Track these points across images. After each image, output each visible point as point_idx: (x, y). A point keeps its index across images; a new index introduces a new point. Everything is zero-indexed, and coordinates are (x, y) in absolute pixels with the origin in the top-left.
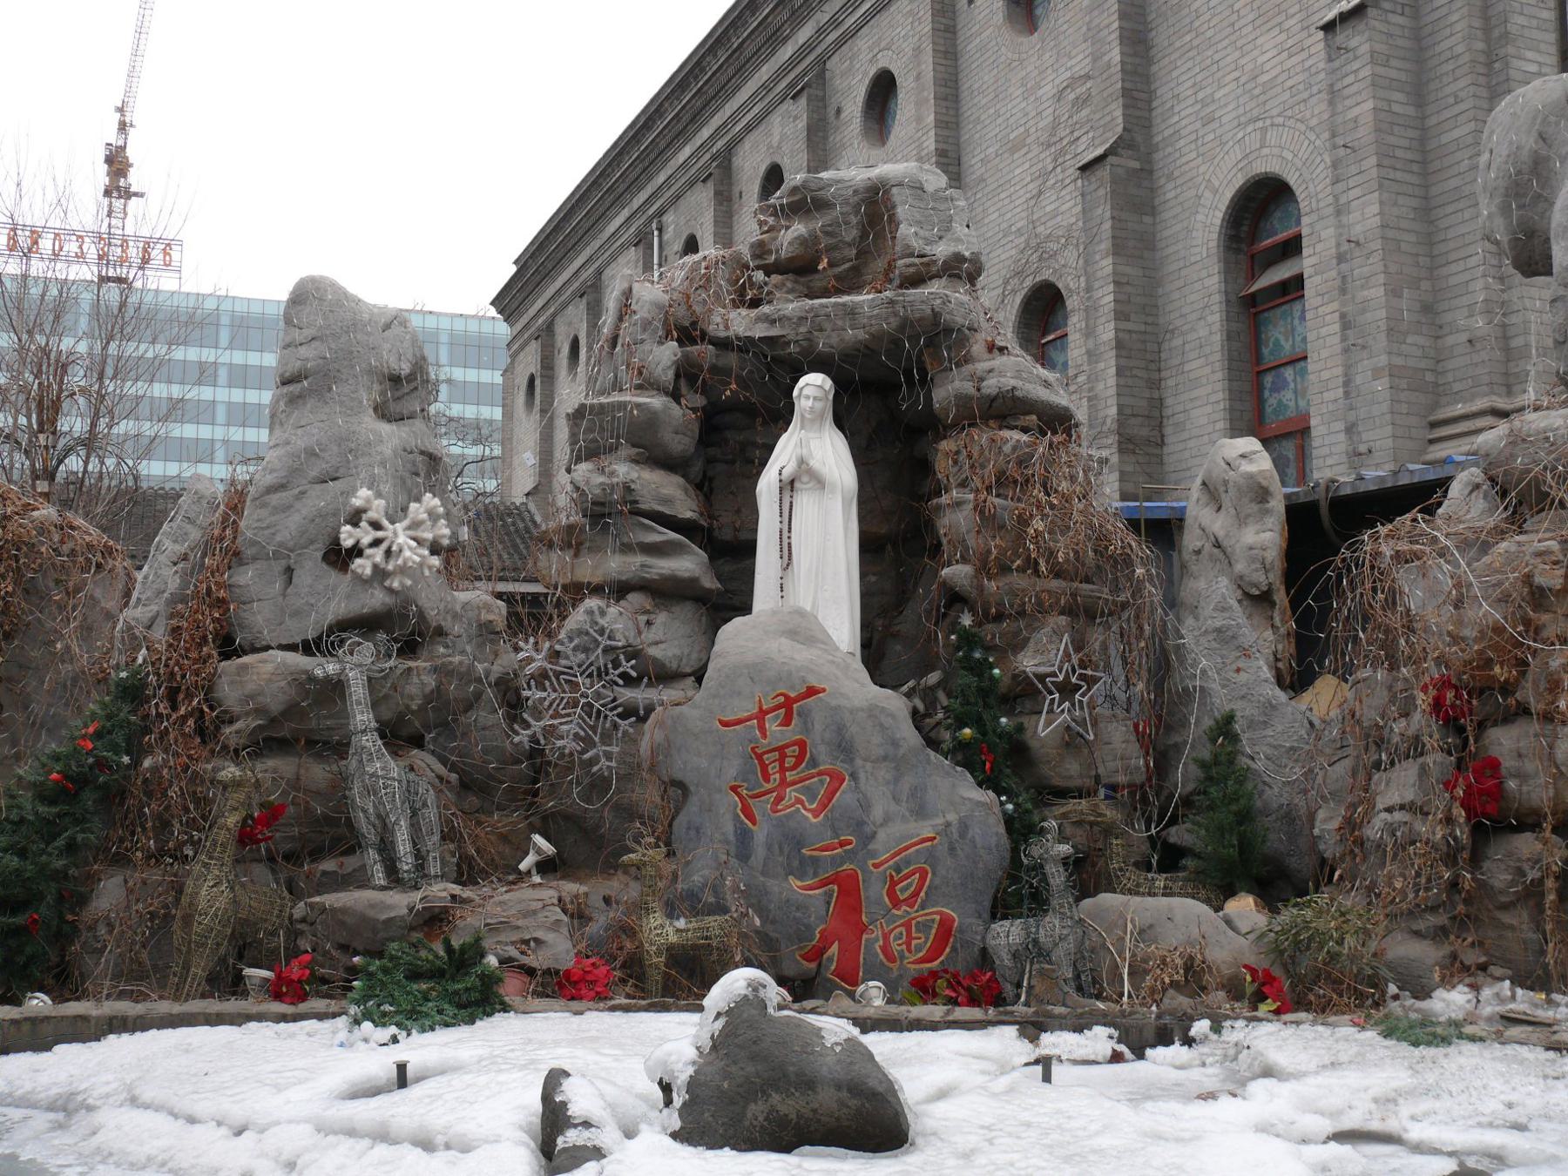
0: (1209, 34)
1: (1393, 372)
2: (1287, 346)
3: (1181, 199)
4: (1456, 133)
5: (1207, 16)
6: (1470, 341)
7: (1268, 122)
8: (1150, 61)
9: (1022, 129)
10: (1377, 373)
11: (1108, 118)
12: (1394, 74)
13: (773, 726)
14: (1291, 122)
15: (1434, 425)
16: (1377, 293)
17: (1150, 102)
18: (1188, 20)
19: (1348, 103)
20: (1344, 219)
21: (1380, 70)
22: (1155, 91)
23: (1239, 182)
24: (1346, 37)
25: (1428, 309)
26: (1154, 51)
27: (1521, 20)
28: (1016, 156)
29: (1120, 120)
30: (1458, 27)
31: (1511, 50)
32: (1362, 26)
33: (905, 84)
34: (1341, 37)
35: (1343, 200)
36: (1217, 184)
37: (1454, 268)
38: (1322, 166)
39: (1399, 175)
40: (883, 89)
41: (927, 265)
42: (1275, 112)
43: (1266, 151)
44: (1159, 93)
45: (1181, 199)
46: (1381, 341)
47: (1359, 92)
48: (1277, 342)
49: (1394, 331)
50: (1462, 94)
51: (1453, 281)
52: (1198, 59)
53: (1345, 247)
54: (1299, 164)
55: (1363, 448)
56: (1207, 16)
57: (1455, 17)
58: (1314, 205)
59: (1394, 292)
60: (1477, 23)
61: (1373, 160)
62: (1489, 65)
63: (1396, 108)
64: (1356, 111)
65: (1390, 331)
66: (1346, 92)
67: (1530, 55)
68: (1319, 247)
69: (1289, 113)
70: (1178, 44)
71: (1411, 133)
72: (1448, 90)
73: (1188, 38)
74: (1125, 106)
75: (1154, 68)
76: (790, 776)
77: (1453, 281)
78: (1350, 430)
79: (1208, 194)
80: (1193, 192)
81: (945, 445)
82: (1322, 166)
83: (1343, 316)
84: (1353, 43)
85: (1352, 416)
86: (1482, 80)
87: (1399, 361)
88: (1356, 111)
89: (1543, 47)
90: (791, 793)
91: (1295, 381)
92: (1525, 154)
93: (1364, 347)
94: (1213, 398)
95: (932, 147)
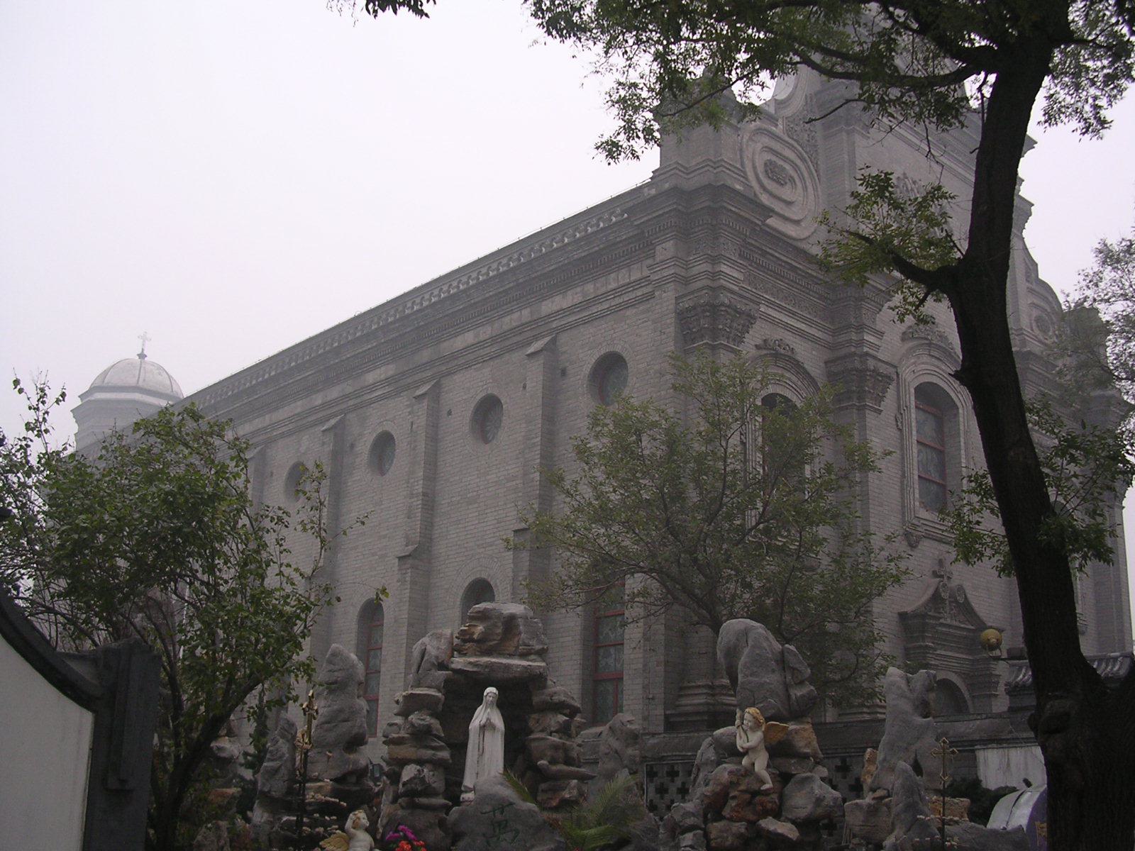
2: (612, 636)
9: (475, 493)
13: (498, 814)
28: (470, 507)
33: (401, 446)
40: (384, 444)
41: (530, 650)
48: (607, 634)
74: (540, 504)
81: (533, 716)
92: (732, 643)
94: (574, 658)
95: (421, 490)
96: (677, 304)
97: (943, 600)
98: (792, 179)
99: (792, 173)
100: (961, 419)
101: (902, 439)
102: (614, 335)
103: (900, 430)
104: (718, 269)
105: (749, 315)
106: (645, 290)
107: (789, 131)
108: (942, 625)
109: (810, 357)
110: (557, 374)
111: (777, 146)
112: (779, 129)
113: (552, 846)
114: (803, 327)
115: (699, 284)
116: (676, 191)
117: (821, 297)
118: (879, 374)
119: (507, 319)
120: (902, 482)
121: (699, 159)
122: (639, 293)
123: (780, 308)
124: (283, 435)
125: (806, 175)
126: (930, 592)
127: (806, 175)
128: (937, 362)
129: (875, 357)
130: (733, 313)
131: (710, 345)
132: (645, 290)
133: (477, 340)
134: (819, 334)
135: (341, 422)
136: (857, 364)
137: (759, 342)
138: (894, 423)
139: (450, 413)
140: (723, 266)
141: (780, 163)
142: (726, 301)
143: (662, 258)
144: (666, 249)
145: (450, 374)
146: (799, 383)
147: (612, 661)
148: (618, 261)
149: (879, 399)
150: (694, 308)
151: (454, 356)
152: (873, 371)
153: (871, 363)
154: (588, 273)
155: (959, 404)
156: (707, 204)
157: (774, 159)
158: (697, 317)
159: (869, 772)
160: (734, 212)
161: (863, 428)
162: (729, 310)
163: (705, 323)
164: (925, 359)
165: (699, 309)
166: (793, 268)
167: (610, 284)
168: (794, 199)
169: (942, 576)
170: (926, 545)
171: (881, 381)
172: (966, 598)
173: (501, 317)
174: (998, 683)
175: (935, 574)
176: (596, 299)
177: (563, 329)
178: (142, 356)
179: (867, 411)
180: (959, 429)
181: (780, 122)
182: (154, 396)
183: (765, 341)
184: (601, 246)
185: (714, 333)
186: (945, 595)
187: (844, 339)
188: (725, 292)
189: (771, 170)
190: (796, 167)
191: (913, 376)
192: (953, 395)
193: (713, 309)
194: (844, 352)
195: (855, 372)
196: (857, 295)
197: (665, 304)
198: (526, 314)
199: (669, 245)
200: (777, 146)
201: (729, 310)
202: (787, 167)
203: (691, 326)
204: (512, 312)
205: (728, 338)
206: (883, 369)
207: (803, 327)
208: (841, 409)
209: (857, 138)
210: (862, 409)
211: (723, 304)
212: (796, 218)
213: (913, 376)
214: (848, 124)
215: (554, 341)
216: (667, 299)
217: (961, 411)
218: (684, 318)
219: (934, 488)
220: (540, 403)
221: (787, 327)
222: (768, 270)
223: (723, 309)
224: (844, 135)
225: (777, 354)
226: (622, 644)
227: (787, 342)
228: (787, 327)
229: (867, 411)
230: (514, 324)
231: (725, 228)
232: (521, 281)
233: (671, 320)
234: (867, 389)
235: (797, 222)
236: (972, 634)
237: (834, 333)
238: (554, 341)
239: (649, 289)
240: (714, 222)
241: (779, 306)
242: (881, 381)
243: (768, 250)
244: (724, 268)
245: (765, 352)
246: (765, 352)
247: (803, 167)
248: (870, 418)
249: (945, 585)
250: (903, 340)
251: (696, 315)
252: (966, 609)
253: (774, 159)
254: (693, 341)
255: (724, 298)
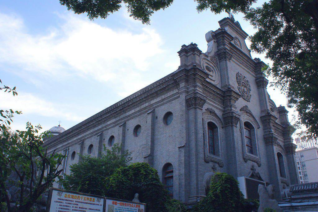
96: (186, 98)
98: (213, 71)
99: (212, 69)
105: (204, 100)
106: (177, 96)
109: (219, 113)
110: (154, 118)
111: (209, 63)
112: (209, 59)
118: (236, 117)
120: (242, 146)
122: (176, 96)
123: (211, 101)
124: (88, 138)
125: (215, 69)
126: (251, 174)
132: (177, 96)
135: (102, 134)
136: (231, 115)
137: (206, 109)
139: (128, 130)
141: (209, 66)
144: (182, 85)
145: (128, 120)
149: (236, 124)
150: (190, 98)
151: (129, 116)
152: (235, 117)
161: (233, 131)
163: (193, 102)
164: (246, 116)
169: (253, 170)
170: (249, 161)
172: (260, 176)
177: (156, 107)
178: (59, 126)
182: (105, 206)
183: (208, 108)
190: (213, 68)
193: (195, 98)
198: (147, 104)
199: (183, 83)
200: (209, 63)
204: (143, 104)
206: (237, 116)
209: (228, 62)
210: (232, 126)
212: (214, 80)
215: (154, 110)
216: (183, 97)
218: (187, 101)
219: (250, 148)
221: (213, 106)
225: (211, 112)
226: (173, 186)
228: (213, 106)
230: (144, 107)
233: (184, 102)
239: (178, 95)
247: (215, 68)
248: (234, 128)
249: (254, 172)
250: (240, 111)
253: (208, 65)
254: (190, 107)
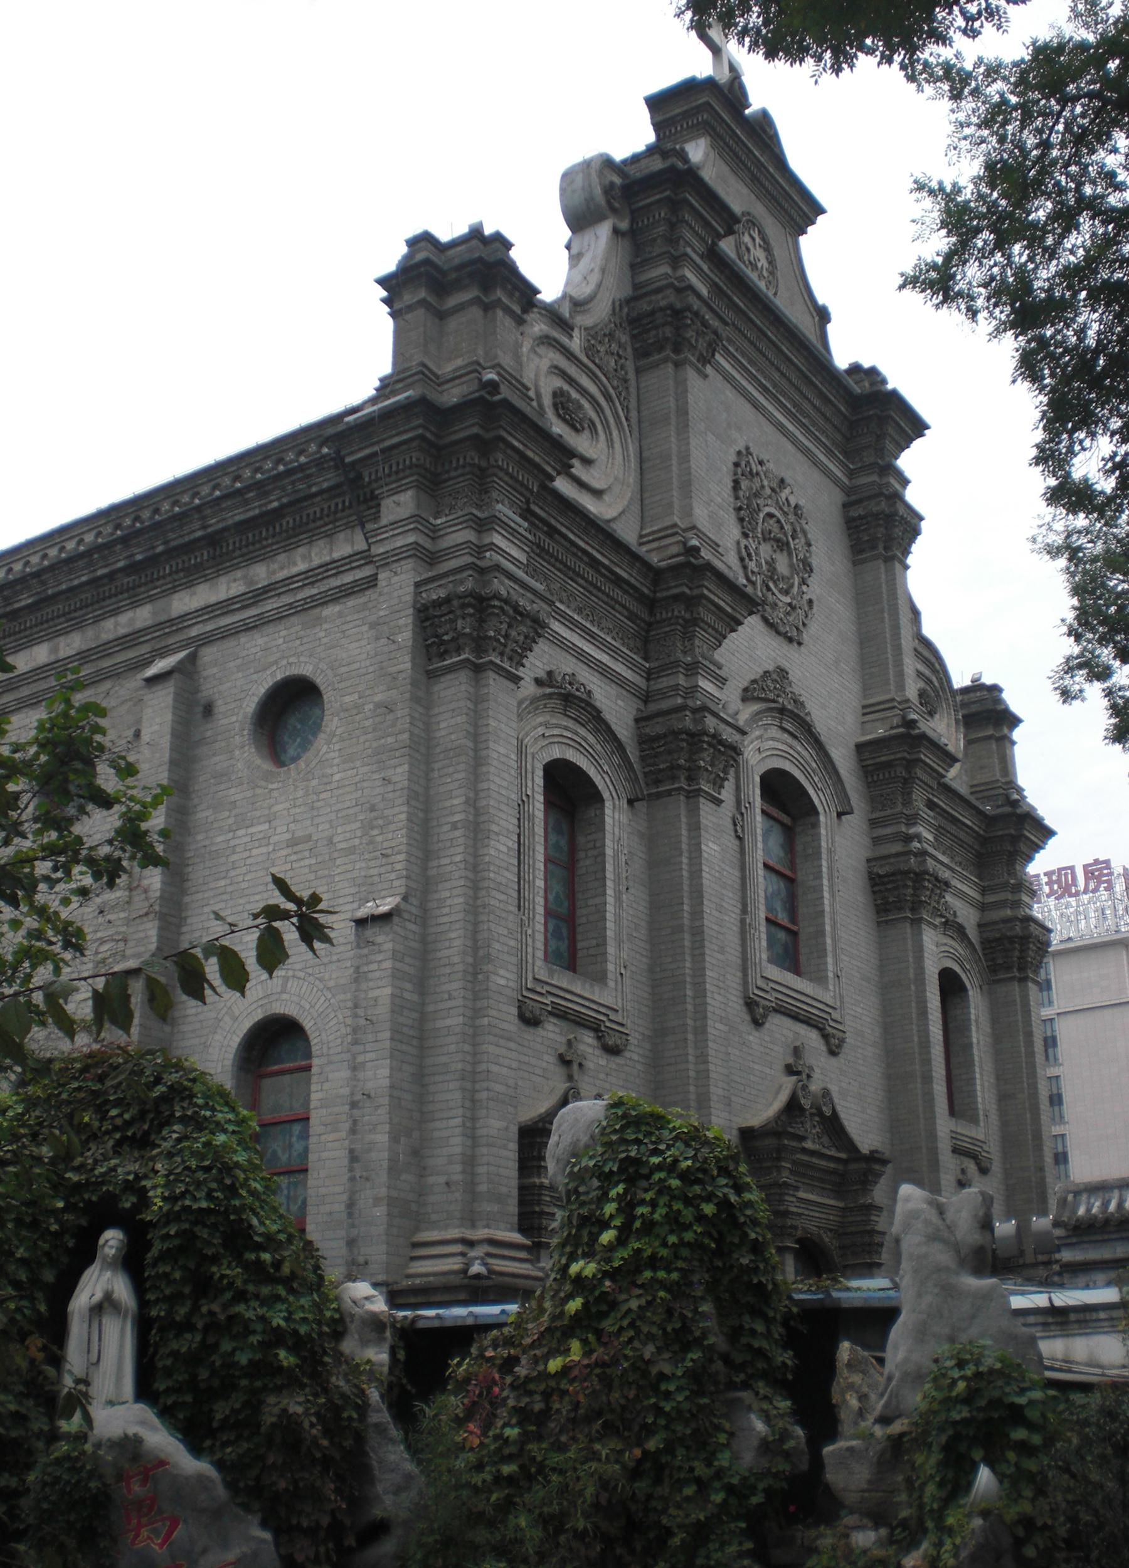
0: (244, 885)
1: (391, 1202)
2: (284, 1158)
3: (201, 1017)
4: (448, 1022)
5: (244, 870)
6: (447, 1184)
7: (290, 973)
8: (183, 892)
10: (377, 1201)
11: (142, 935)
12: (407, 968)
14: (311, 979)
15: (416, 1245)
16: (382, 1138)
17: (179, 926)
18: (224, 868)
19: (371, 984)
20: (361, 1075)
21: (399, 965)
22: (186, 918)
23: (258, 1016)
24: (374, 933)
25: (416, 1153)
26: (189, 884)
27: (497, 946)
29: (154, 939)
30: (457, 943)
31: (490, 967)
32: (387, 929)
34: (370, 932)
35: (360, 1059)
36: (237, 1013)
37: (438, 1124)
38: (335, 1021)
39: (404, 1047)
42: (298, 966)
43: (285, 996)
44: (189, 921)
45: (201, 1017)
46: (383, 1177)
47: (380, 978)
49: (394, 1169)
50: (455, 994)
51: (437, 1134)
52: (230, 903)
53: (358, 1097)
54: (315, 1015)
55: (361, 1259)
56: (244, 870)
57: (453, 935)
58: (325, 1051)
59: (394, 1139)
60: (469, 943)
61: (388, 1034)
62: (475, 974)
63: (407, 995)
64: (376, 993)
65: (391, 1169)
66: (370, 975)
67: (502, 972)
68: (326, 1086)
69: (310, 971)
70: (212, 885)
71: (415, 1015)
72: (445, 988)
73: (223, 883)
74: (160, 928)
75: (187, 899)
76: (144, 1520)
77: (437, 1134)
78: (351, 1243)
79: (227, 1019)
80: (213, 1015)
82: (335, 1021)
83: (351, 1151)
84: (380, 939)
85: (354, 1232)
86: (469, 985)
87: (394, 1194)
88: (376, 993)
89: (510, 967)
90: (144, 1533)
91: (288, 1188)
93: (367, 1179)
96: (417, 594)
97: (802, 1109)
99: (592, 414)
100: (823, 832)
101: (742, 851)
102: (301, 649)
103: (738, 837)
104: (487, 541)
106: (359, 574)
107: (590, 351)
108: (804, 1150)
111: (572, 370)
112: (576, 344)
113: (245, 1549)
114: (604, 658)
115: (453, 564)
116: (422, 405)
117: (632, 616)
118: (721, 742)
119: (109, 624)
121: (459, 362)
125: (611, 420)
126: (783, 1098)
127: (611, 420)
128: (790, 740)
129: (715, 715)
130: (511, 612)
131: (473, 663)
132: (359, 574)
133: (53, 658)
134: (628, 674)
136: (688, 722)
137: (541, 674)
138: (731, 827)
140: (496, 535)
141: (574, 395)
142: (504, 592)
143: (392, 518)
146: (599, 747)
147: (283, 1200)
148: (312, 526)
149: (719, 783)
150: (448, 600)
152: (714, 736)
153: (711, 722)
154: (258, 546)
155: (820, 809)
156: (475, 430)
157: (566, 387)
158: (451, 616)
159: (851, 1387)
160: (514, 448)
162: (506, 608)
163: (465, 626)
164: (774, 732)
165: (455, 603)
166: (594, 563)
167: (295, 564)
168: (595, 456)
169: (798, 1073)
171: (723, 753)
173: (98, 620)
174: (881, 1245)
175: (790, 1070)
176: (268, 590)
179: (702, 800)
180: (820, 846)
181: (576, 333)
184: (285, 500)
185: (480, 644)
186: (806, 1103)
187: (665, 684)
188: (503, 578)
189: (561, 401)
191: (758, 757)
192: (811, 792)
194: (665, 705)
195: (684, 736)
196: (688, 616)
197: (396, 594)
200: (572, 370)
201: (506, 608)
202: (583, 402)
203: (440, 631)
205: (502, 654)
207: (604, 658)
208: (659, 796)
210: (693, 795)
211: (496, 596)
213: (758, 757)
214: (677, 350)
215: (192, 658)
217: (822, 818)
219: (782, 935)
220: (166, 758)
222: (557, 559)
223: (496, 603)
224: (670, 368)
227: (582, 680)
229: (702, 800)
231: (501, 474)
232: (139, 557)
233: (406, 620)
234: (702, 763)
235: (597, 493)
236: (841, 1167)
237: (649, 676)
238: (192, 658)
239: (367, 571)
240: (484, 464)
241: (571, 620)
242: (723, 753)
243: (559, 526)
244: (498, 540)
245: (548, 690)
246: (548, 690)
248: (706, 808)
251: (450, 612)
252: (833, 1126)
253: (566, 387)
254: (442, 656)
255: (501, 586)
